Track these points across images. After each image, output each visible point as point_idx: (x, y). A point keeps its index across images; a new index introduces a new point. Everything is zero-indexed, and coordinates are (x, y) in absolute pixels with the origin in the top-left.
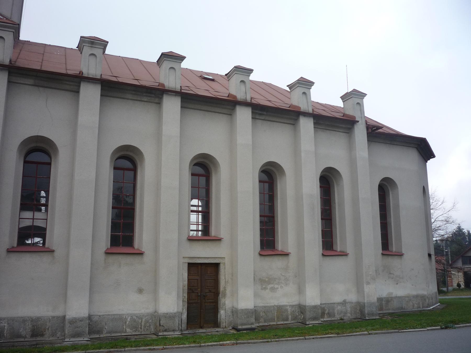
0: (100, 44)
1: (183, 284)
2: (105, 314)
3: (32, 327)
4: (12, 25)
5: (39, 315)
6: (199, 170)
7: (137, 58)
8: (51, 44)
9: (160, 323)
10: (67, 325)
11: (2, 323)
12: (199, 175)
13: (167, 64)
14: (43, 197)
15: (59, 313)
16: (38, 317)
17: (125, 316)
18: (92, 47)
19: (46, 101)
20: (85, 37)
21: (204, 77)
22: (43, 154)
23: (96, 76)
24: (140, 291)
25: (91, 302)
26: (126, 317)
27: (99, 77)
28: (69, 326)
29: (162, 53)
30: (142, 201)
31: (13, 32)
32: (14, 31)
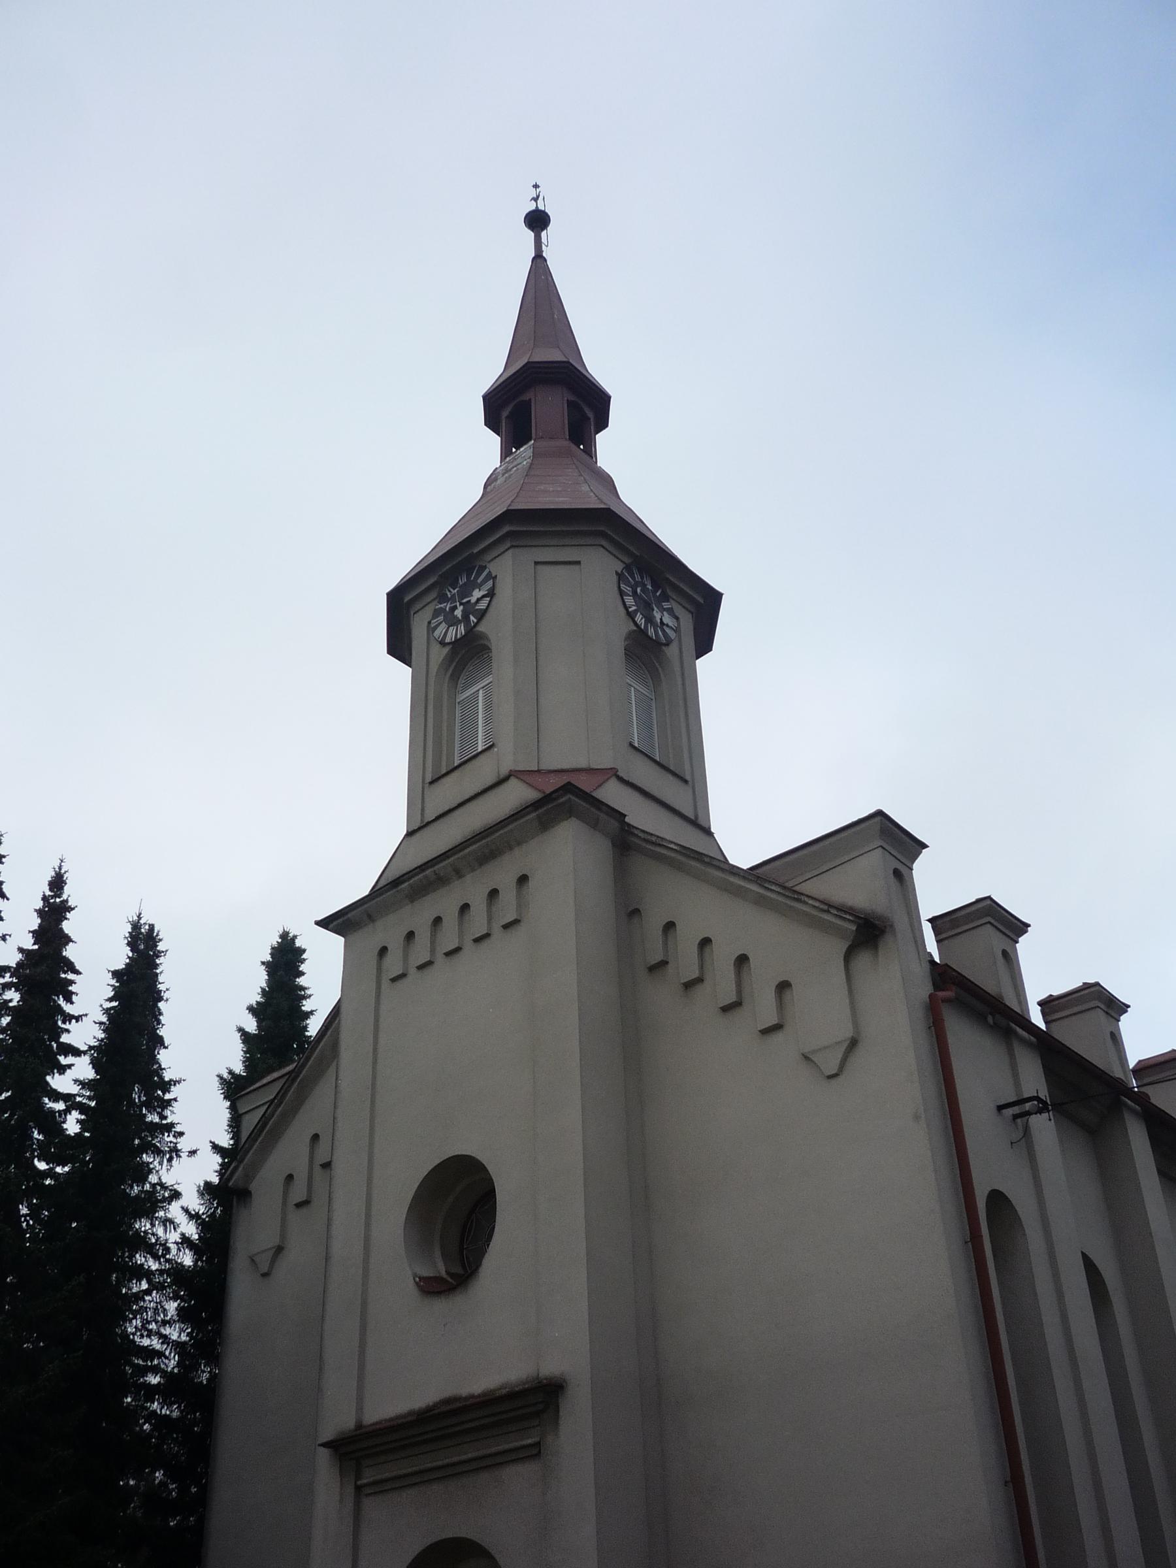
31: (990, 923)
32: (989, 919)
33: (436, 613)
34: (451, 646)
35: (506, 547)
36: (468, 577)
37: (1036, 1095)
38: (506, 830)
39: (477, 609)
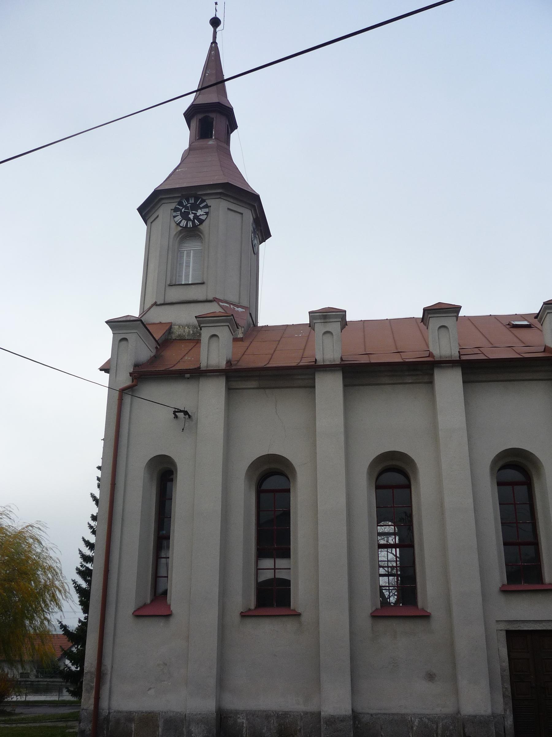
0: (336, 317)
1: (501, 666)
2: (379, 712)
3: (278, 727)
4: (225, 318)
5: (287, 710)
6: (512, 475)
7: (412, 317)
8: (294, 324)
9: (464, 731)
10: (323, 727)
11: (239, 717)
12: (513, 484)
13: (435, 323)
14: (398, 561)
15: (311, 707)
16: (285, 712)
17: (409, 717)
18: (327, 322)
19: (275, 406)
20: (316, 312)
21: (513, 324)
22: (271, 478)
23: (334, 361)
24: (431, 677)
25: (354, 691)
26: (411, 718)
27: (338, 362)
28: (325, 728)
29: (423, 309)
30: (421, 534)
31: (228, 326)
32: (228, 324)
33: (176, 210)
36: (196, 201)
37: (184, 410)
39: (200, 218)
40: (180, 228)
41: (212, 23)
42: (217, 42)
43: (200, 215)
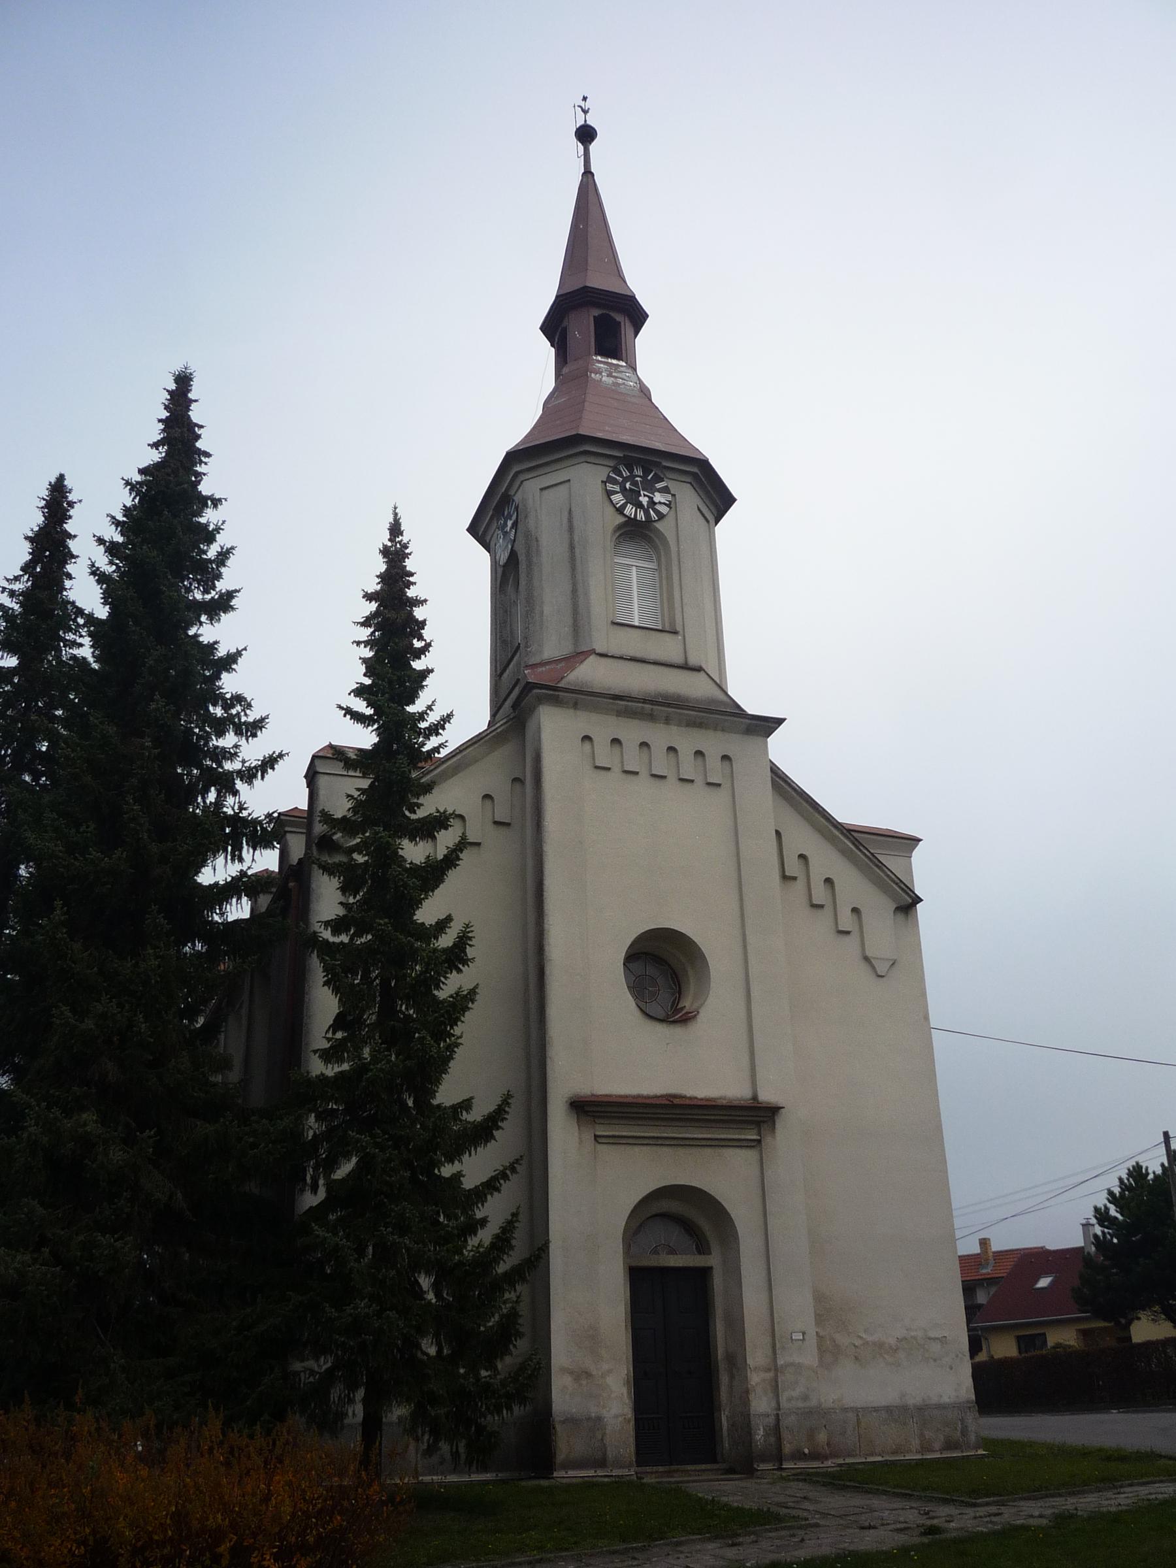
34: (627, 519)
35: (687, 480)
38: (723, 717)
40: (621, 519)
41: (579, 136)
42: (592, 171)
43: (660, 503)
